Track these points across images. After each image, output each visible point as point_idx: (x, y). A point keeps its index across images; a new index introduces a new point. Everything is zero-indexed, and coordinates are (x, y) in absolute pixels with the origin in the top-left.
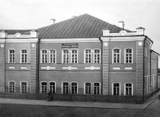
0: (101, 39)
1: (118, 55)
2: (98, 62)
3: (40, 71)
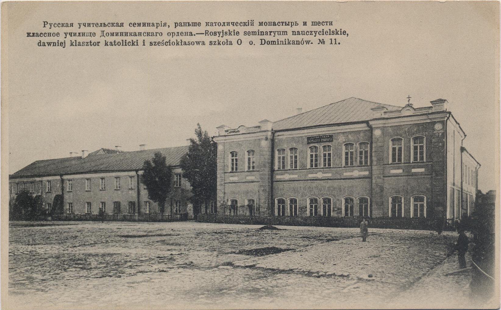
0: (370, 124)
2: (366, 162)
3: (274, 183)
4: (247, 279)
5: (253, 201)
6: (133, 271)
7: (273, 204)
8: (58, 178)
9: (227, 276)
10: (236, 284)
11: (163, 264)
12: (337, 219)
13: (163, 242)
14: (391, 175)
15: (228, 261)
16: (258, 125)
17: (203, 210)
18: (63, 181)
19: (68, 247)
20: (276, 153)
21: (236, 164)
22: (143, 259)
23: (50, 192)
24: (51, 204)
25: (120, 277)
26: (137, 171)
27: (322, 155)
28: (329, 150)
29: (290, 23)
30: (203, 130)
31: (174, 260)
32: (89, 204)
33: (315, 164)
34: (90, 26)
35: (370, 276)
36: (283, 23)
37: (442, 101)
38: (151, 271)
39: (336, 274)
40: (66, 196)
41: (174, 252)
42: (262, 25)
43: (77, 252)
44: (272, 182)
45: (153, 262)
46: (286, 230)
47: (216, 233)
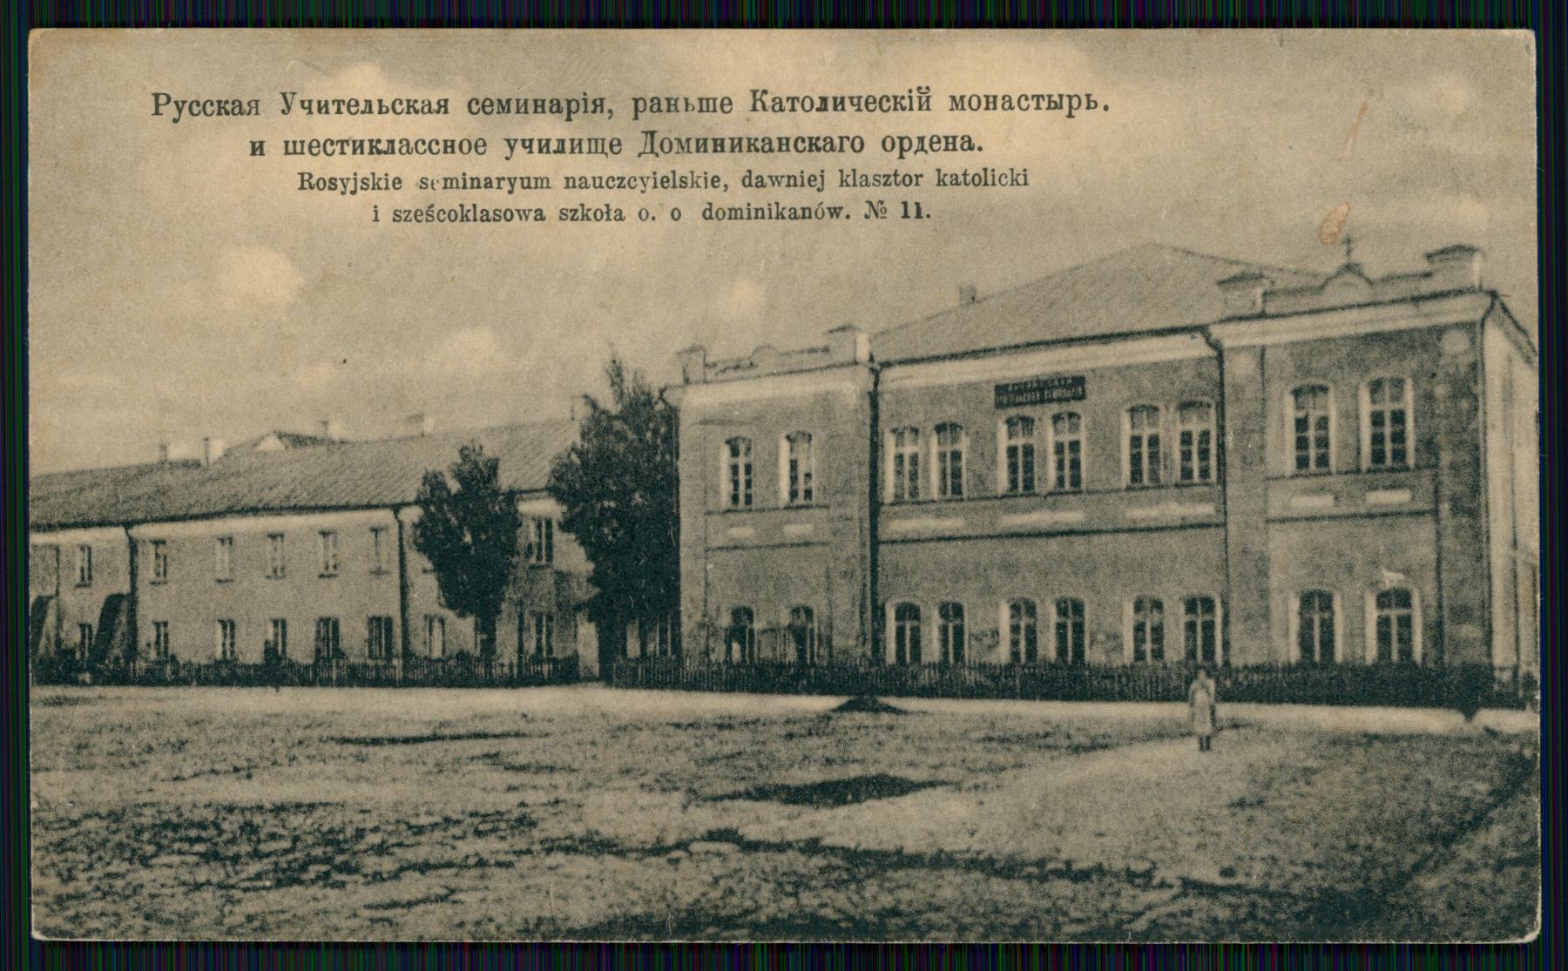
0: (1214, 337)
1: (1394, 413)
2: (1205, 473)
4: (789, 889)
5: (809, 612)
6: (387, 865)
7: (879, 613)
8: (119, 532)
9: (721, 877)
10: (748, 904)
11: (492, 838)
12: (1108, 674)
13: (493, 758)
14: (1295, 515)
15: (723, 824)
16: (820, 342)
17: (633, 647)
18: (133, 546)
19: (154, 778)
20: (889, 442)
21: (748, 484)
22: (424, 820)
23: (86, 586)
24: (90, 626)
25: (342, 885)
26: (396, 508)
27: (1051, 449)
28: (1074, 428)
29: (1065, 100)
30: (630, 366)
31: (533, 824)
32: (229, 626)
33: (1024, 483)
34: (327, 112)
35: (1227, 872)
36: (1038, 97)
37: (1463, 251)
38: (449, 865)
39: (1106, 866)
40: (145, 597)
41: (531, 797)
42: (963, 109)
43: (188, 799)
44: (875, 542)
45: (457, 831)
46: (925, 713)
47: (678, 726)
